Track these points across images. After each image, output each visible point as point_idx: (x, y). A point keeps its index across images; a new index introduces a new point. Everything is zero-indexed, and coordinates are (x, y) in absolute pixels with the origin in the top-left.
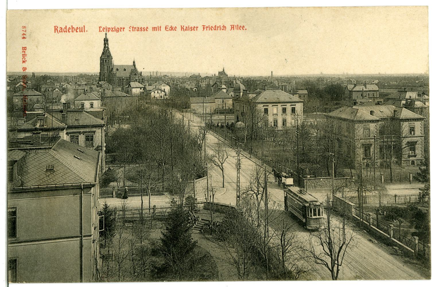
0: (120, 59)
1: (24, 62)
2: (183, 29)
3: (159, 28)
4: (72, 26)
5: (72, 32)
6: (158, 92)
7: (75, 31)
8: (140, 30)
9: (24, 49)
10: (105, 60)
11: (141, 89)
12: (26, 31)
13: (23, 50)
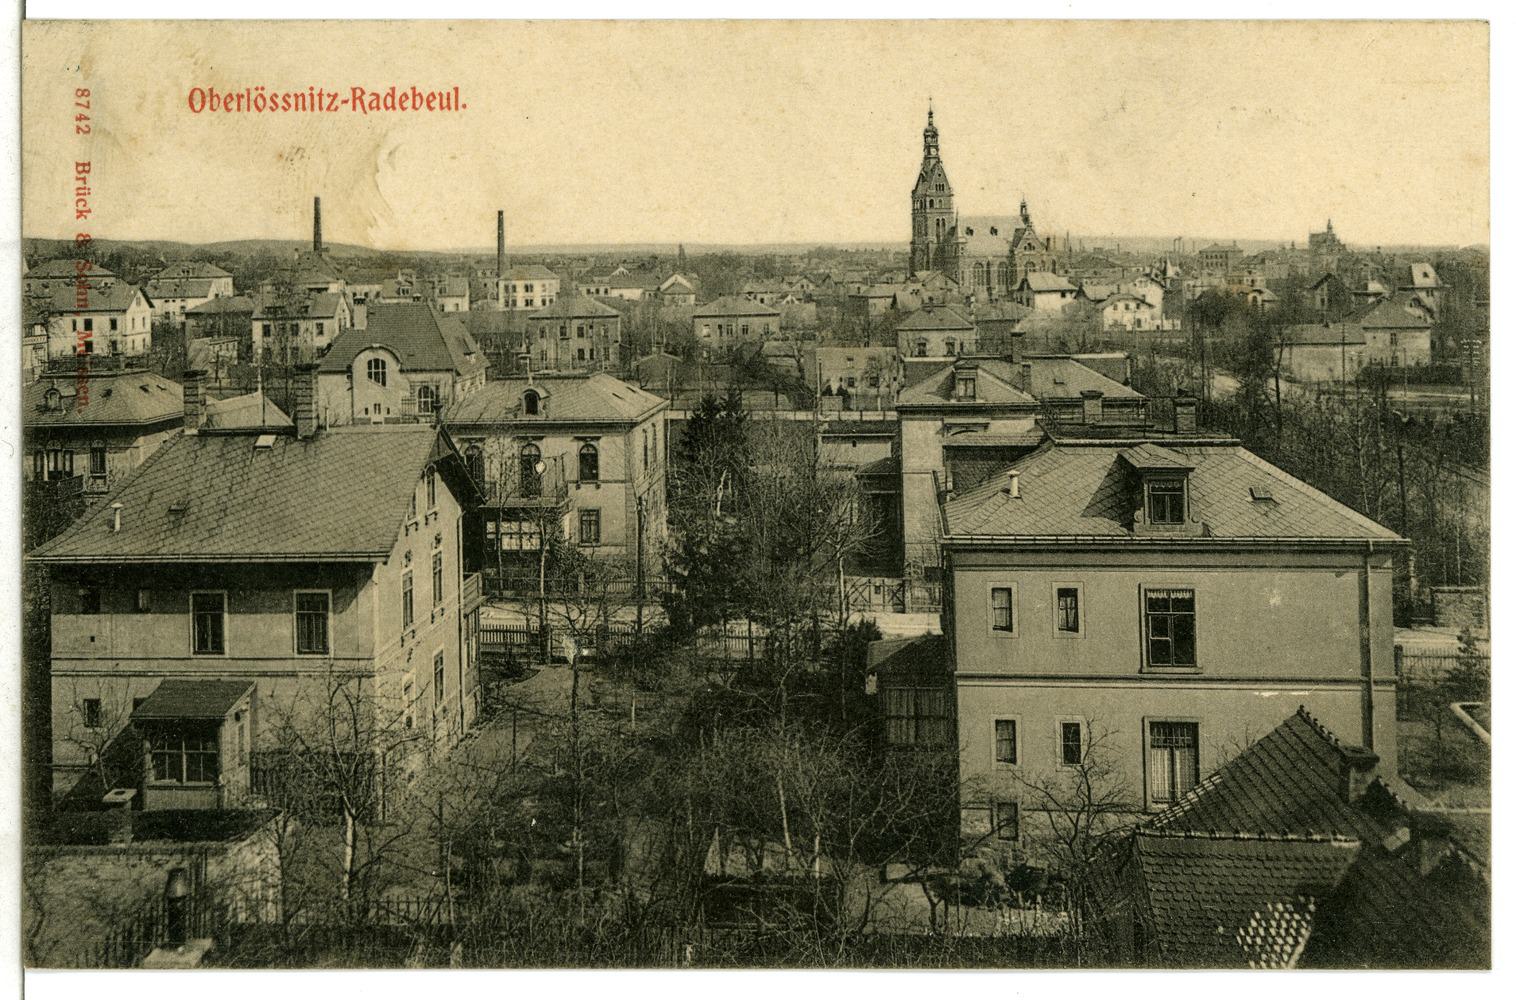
0: (978, 198)
1: (80, 214)
2: (362, 103)
3: (316, 99)
4: (414, 89)
5: (414, 107)
6: (1127, 307)
7: (425, 103)
8: (292, 101)
9: (84, 168)
10: (928, 199)
11: (1063, 295)
12: (88, 107)
13: (79, 172)
